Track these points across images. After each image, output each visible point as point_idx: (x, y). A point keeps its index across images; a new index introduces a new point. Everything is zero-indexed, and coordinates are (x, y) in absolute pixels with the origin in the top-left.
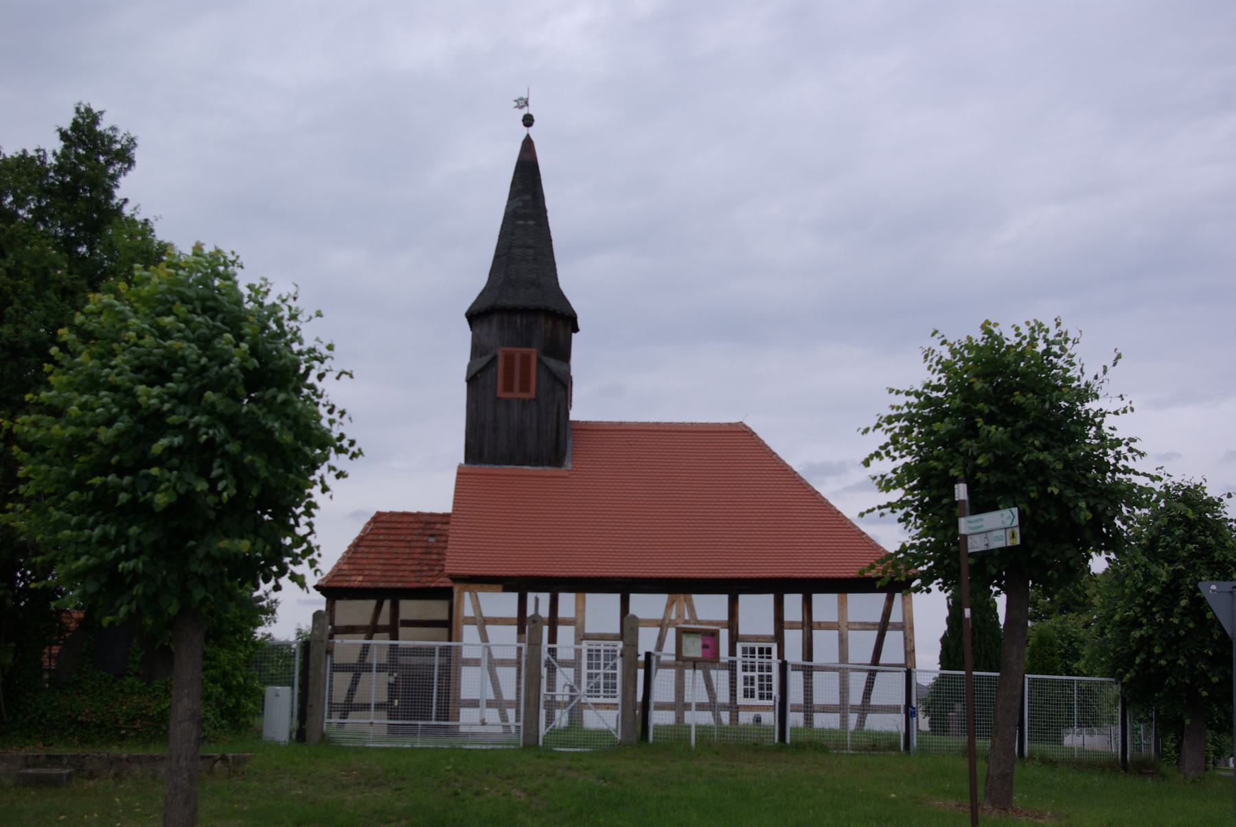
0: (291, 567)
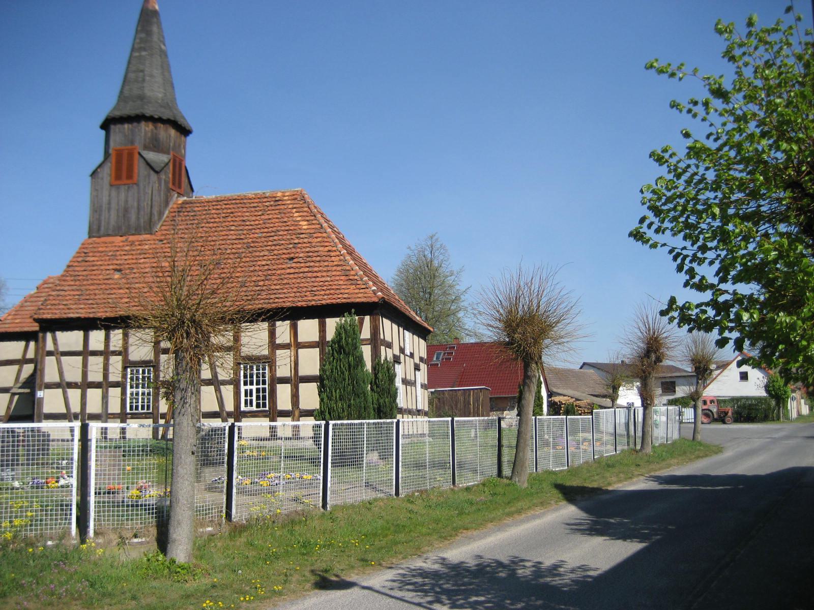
0: (765, 100)
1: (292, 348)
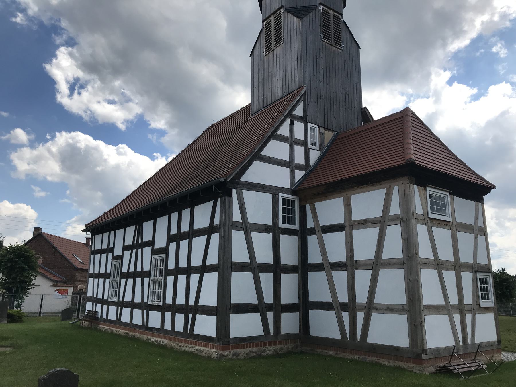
1: (347, 229)
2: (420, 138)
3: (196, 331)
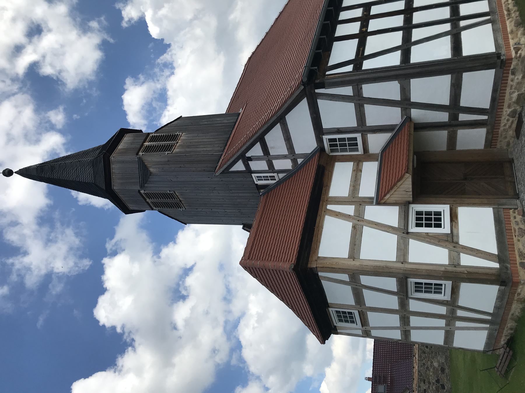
2: (278, 279)
3: (486, 105)
